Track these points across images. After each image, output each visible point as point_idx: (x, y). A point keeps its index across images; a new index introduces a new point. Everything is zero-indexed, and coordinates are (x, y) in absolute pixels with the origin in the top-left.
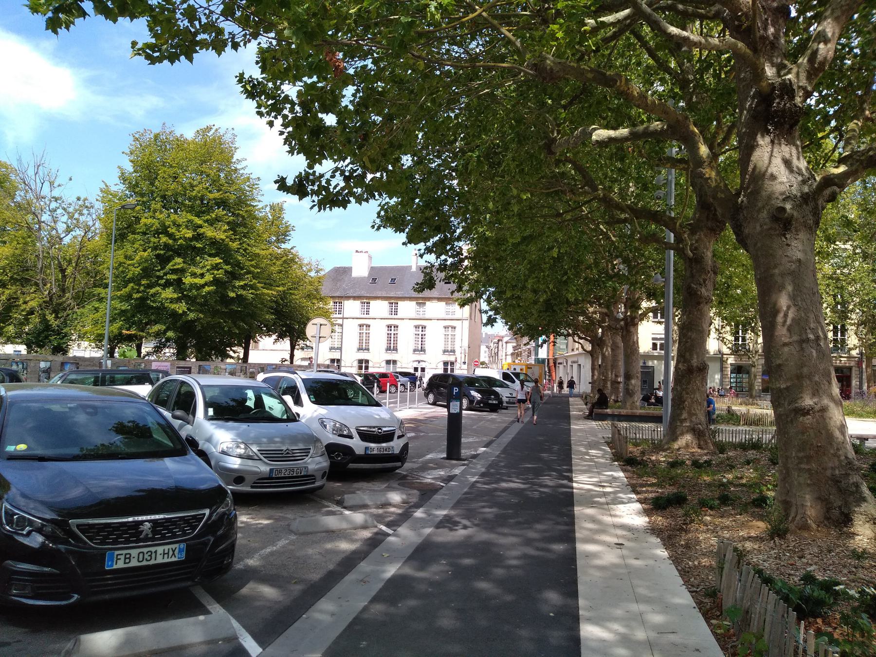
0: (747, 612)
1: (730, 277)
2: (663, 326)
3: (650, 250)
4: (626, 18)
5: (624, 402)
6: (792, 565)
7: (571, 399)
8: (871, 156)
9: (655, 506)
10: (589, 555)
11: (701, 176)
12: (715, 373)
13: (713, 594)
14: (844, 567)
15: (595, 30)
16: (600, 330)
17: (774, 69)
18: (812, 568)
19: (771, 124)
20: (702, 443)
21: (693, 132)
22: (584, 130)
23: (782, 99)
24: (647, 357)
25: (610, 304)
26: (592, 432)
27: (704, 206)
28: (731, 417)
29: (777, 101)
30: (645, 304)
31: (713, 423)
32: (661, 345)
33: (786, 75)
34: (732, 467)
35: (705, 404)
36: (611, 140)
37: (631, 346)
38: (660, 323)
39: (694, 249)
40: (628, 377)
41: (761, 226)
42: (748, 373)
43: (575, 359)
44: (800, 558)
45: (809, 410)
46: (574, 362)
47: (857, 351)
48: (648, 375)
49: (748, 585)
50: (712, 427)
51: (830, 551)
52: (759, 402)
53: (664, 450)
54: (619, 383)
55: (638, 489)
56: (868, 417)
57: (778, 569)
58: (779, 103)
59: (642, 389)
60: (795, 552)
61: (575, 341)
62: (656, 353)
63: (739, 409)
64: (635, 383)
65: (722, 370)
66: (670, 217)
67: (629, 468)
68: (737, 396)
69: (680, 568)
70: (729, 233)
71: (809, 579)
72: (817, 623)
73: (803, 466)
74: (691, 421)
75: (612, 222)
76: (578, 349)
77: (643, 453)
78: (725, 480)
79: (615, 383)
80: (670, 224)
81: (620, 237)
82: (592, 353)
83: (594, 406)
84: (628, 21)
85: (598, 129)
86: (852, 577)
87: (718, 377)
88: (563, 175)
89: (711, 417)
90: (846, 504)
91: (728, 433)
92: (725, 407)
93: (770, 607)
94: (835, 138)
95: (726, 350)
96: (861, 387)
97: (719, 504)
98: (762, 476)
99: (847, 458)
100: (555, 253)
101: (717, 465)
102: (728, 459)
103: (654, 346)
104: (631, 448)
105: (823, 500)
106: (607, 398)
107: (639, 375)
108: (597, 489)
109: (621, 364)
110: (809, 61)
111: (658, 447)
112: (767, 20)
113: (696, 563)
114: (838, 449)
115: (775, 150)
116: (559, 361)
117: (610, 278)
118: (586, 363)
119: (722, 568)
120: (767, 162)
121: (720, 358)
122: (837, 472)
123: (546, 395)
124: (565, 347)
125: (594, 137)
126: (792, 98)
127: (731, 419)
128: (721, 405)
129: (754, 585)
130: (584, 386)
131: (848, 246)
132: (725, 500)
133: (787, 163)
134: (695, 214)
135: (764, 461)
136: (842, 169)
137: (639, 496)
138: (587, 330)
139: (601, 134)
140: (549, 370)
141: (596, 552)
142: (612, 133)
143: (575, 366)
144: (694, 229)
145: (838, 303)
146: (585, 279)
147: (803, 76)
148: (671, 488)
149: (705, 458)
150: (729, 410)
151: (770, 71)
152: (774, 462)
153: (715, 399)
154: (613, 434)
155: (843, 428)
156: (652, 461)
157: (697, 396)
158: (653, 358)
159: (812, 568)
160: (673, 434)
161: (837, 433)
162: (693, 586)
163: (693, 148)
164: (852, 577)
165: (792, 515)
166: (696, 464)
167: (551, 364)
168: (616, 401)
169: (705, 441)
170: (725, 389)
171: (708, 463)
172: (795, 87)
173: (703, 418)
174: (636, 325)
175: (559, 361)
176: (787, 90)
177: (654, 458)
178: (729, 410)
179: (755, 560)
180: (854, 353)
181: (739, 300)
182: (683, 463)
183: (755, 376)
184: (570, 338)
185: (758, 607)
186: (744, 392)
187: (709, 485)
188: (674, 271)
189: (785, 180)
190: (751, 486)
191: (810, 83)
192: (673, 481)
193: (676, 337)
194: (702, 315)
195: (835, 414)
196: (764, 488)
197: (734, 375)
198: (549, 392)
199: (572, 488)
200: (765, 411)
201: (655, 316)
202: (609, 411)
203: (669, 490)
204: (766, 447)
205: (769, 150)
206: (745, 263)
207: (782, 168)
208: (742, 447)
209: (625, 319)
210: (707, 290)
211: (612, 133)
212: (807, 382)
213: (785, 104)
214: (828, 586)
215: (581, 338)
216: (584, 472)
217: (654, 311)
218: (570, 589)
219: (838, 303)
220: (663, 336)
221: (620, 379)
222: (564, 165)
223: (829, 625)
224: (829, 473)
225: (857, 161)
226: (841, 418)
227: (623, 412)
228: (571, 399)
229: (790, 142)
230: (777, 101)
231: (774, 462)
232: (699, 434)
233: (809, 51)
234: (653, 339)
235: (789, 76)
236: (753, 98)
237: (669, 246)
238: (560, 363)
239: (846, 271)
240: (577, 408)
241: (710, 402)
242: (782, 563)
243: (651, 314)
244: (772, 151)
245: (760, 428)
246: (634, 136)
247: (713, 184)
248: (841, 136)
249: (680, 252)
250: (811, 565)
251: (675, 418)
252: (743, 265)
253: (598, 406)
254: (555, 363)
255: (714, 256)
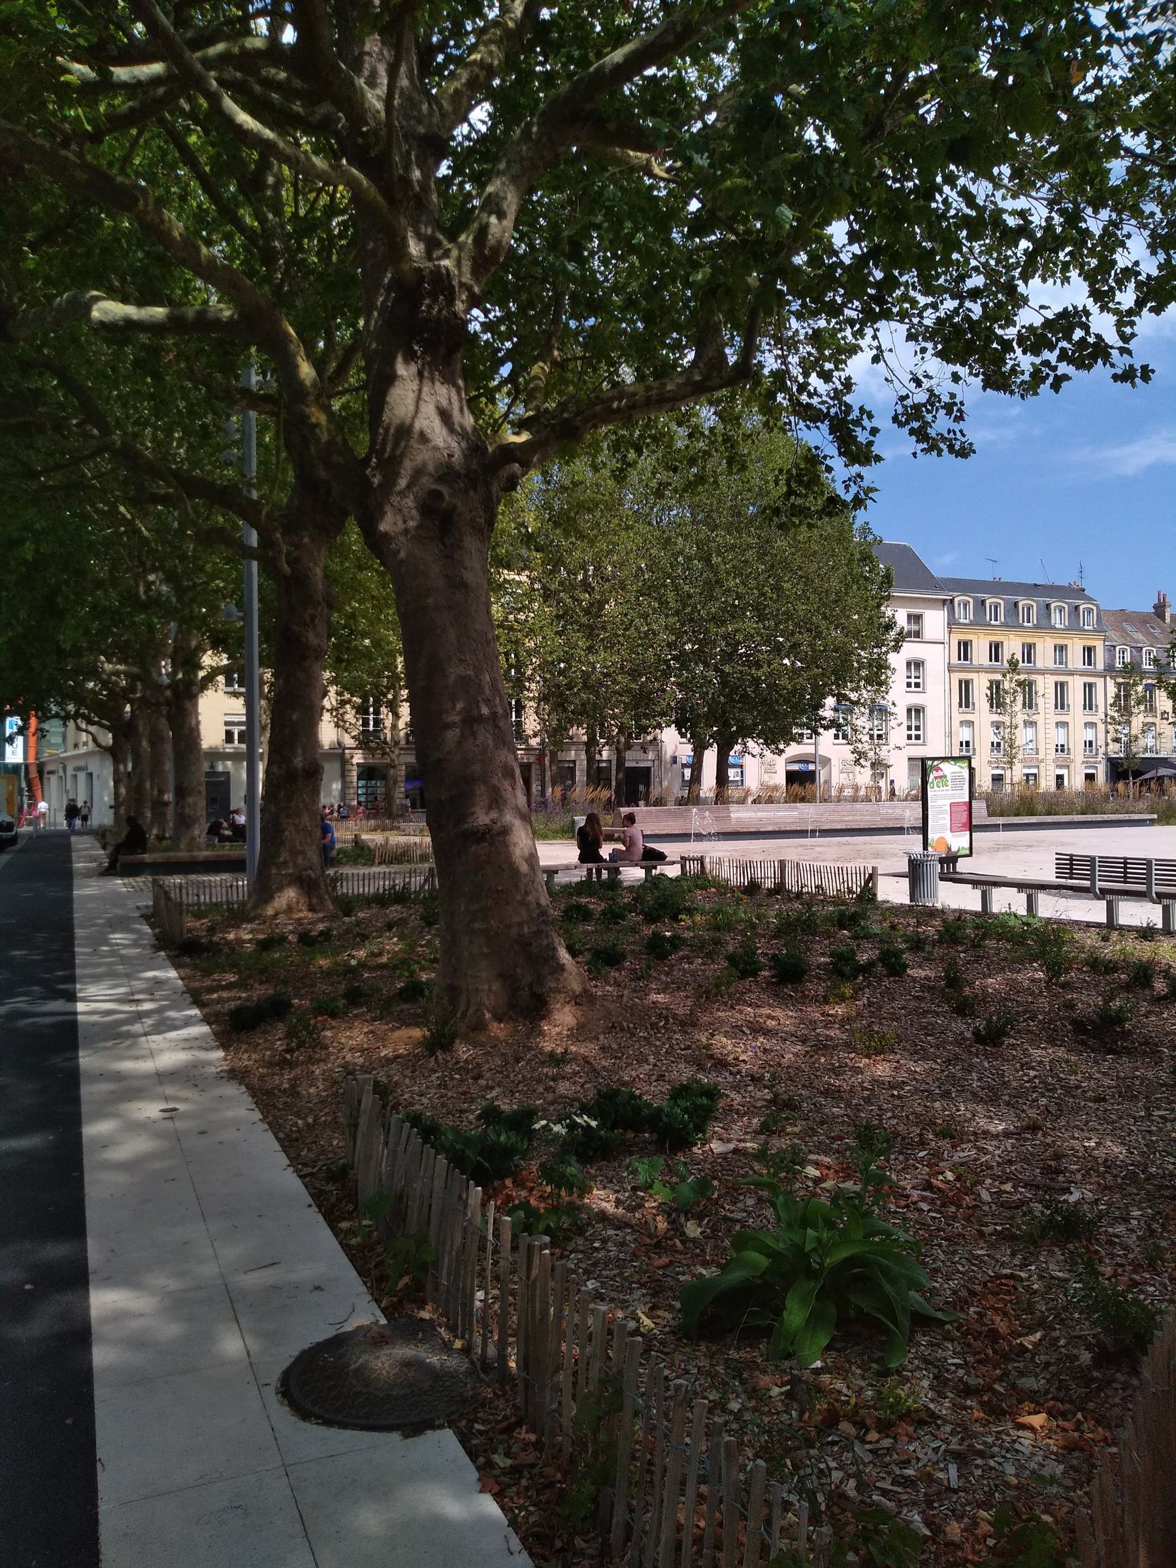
0: (400, 1198)
1: (353, 616)
2: (241, 700)
3: (215, 560)
4: (155, 81)
5: (176, 839)
6: (464, 1093)
7: (73, 839)
8: (567, 420)
9: (233, 1027)
10: (105, 1143)
11: (304, 418)
12: (331, 781)
13: (341, 1175)
14: (539, 1081)
15: (88, 92)
16: (128, 708)
17: (422, 246)
18: (494, 1094)
19: (418, 343)
20: (314, 901)
21: (286, 335)
22: (74, 297)
23: (435, 300)
24: (215, 755)
25: (141, 655)
26: (115, 899)
27: (307, 484)
28: (361, 853)
29: (427, 301)
30: (209, 660)
31: (332, 866)
32: (241, 734)
33: (439, 259)
34: (364, 937)
35: (319, 833)
36: (130, 324)
37: (188, 735)
38: (235, 695)
39: (293, 562)
40: (181, 793)
41: (405, 522)
42: (384, 777)
43: (81, 763)
44: (476, 1079)
45: (484, 833)
46: (78, 769)
47: (538, 740)
48: (219, 788)
49: (401, 1149)
50: (331, 872)
51: (518, 1060)
52: (403, 825)
53: (250, 921)
54: (166, 804)
55: (206, 997)
56: (555, 838)
57: (443, 1105)
58: (430, 307)
59: (209, 815)
60: (468, 1071)
61: (79, 729)
62: (229, 748)
63: (373, 838)
64: (198, 804)
65: (344, 775)
66: (249, 500)
67: (187, 960)
68: (368, 818)
69: (281, 1135)
70: (353, 536)
71: (491, 1115)
72: (506, 1187)
73: (477, 926)
74: (295, 865)
75: (139, 502)
76: (85, 744)
77: (212, 930)
78: (353, 962)
79: (159, 805)
80: (250, 512)
81: (158, 531)
82: (114, 753)
83: (118, 850)
84: (161, 90)
85: (102, 299)
86: (550, 1097)
87: (336, 786)
88: (38, 393)
89: (328, 856)
90: (540, 980)
91: (359, 880)
92: (350, 837)
93: (438, 1184)
94: (509, 394)
95: (348, 741)
96: (543, 792)
97: (345, 1006)
98: (412, 947)
99: (539, 905)
100: (28, 551)
101: (340, 937)
102: (358, 923)
103: (229, 736)
104: (190, 923)
105: (508, 978)
106: (143, 833)
107: (203, 788)
108: (127, 1008)
109: (169, 766)
110: (475, 240)
111: (236, 915)
112: (408, 153)
113: (310, 1120)
114: (527, 893)
115: (425, 389)
116: (49, 768)
117: (144, 607)
118: (104, 771)
119: (356, 1126)
120: (412, 408)
121: (339, 754)
122: (526, 930)
123: (23, 835)
124: (59, 740)
125: (95, 314)
126: (451, 301)
127: (359, 856)
128: (343, 834)
129: (410, 1148)
130: (102, 815)
131: (523, 578)
132: (355, 997)
133: (445, 415)
134: (291, 498)
135: (415, 921)
136: (524, 437)
137: (206, 1010)
138: (103, 710)
139: (108, 309)
140: (30, 789)
141: (118, 1138)
142: (131, 311)
143: (82, 777)
144: (291, 523)
145: (511, 666)
146: (94, 608)
147: (467, 266)
148: (264, 987)
149: (321, 927)
150: (357, 842)
151: (415, 248)
152: (429, 921)
153: (333, 824)
154: (156, 900)
155: (532, 858)
156: (228, 943)
157: (306, 820)
158: (225, 756)
159: (494, 1094)
160: (264, 890)
161: (524, 868)
162: (305, 1165)
163: (287, 369)
164: (550, 1097)
165: (462, 1008)
166: (306, 939)
167: (34, 774)
168: (160, 838)
169: (320, 898)
170: (350, 807)
171: (326, 935)
172: (455, 283)
173: (314, 857)
174: (193, 698)
175: (49, 768)
176: (442, 284)
177: (231, 936)
178: (357, 842)
179: (407, 1096)
180: (534, 742)
181: (367, 655)
182: (282, 939)
183: (395, 782)
184: (71, 724)
185: (417, 1186)
186: (380, 810)
187: (328, 974)
188: (260, 600)
189: (442, 445)
190: (395, 967)
191: (478, 281)
192: (266, 974)
193: (265, 719)
194: (311, 680)
195: (521, 838)
196: (416, 967)
197: (361, 783)
198: (30, 828)
199: (75, 1013)
200: (417, 839)
201: (229, 683)
202: (147, 857)
203: (261, 992)
204: (416, 898)
205: (415, 388)
206: (375, 593)
207: (437, 423)
208: (380, 900)
209: (174, 685)
210: (317, 635)
211: (131, 311)
212: (480, 790)
213: (440, 311)
214: (521, 1121)
215: (90, 722)
216: (97, 978)
217: (227, 671)
218: (72, 1222)
219: (511, 666)
220: (244, 719)
221: (169, 797)
222: (41, 375)
223: (524, 1187)
224: (514, 932)
225: (546, 427)
226: (530, 842)
227: (183, 855)
228: (73, 839)
229: (449, 380)
230: (427, 301)
231: (429, 921)
232: (309, 887)
233: (476, 225)
234: (227, 723)
235: (445, 262)
236: (389, 289)
237: (247, 553)
238: (50, 773)
239: (522, 616)
240: (87, 854)
241: (326, 830)
242: (450, 1094)
243: (221, 679)
244: (420, 391)
245: (406, 867)
246: (175, 324)
247: (325, 437)
248: (518, 392)
249: (269, 567)
250: (492, 1088)
251: (268, 858)
252: (373, 597)
253: (127, 851)
254: (41, 772)
255: (326, 577)
